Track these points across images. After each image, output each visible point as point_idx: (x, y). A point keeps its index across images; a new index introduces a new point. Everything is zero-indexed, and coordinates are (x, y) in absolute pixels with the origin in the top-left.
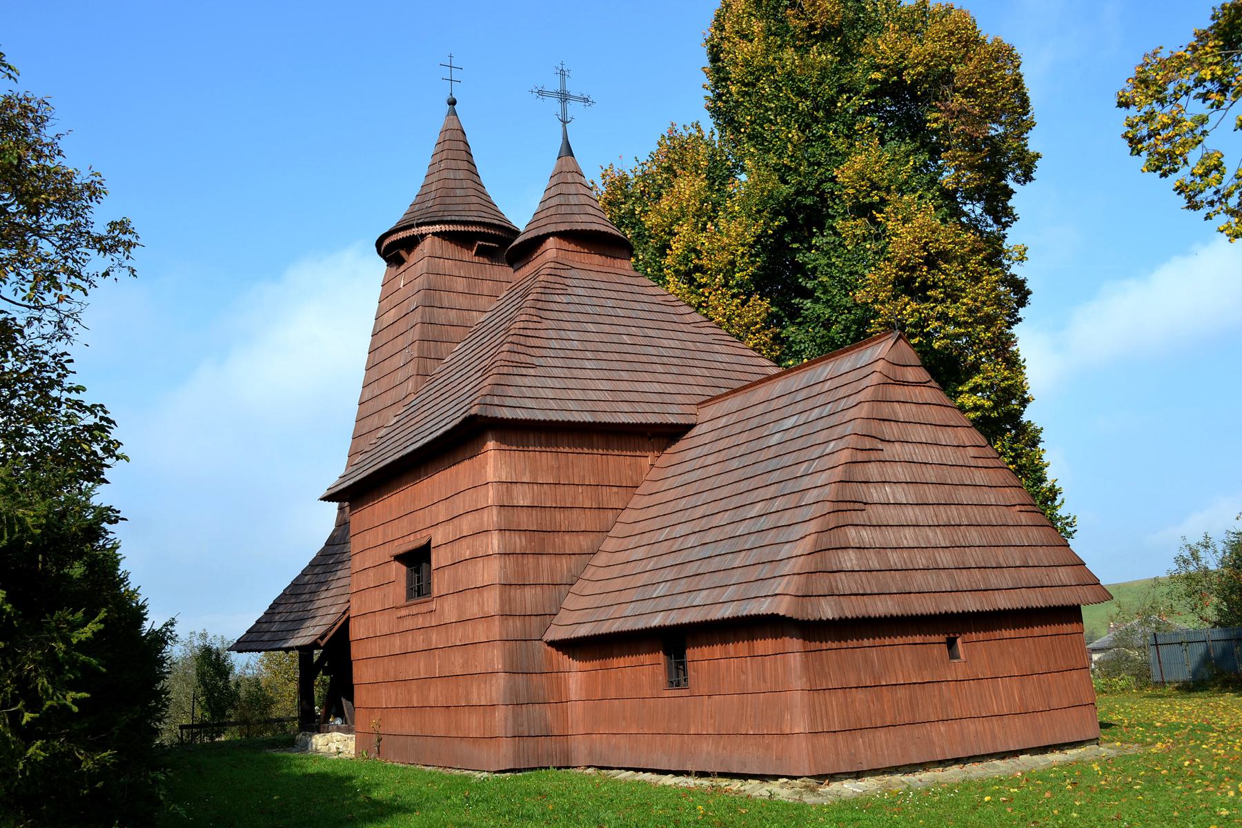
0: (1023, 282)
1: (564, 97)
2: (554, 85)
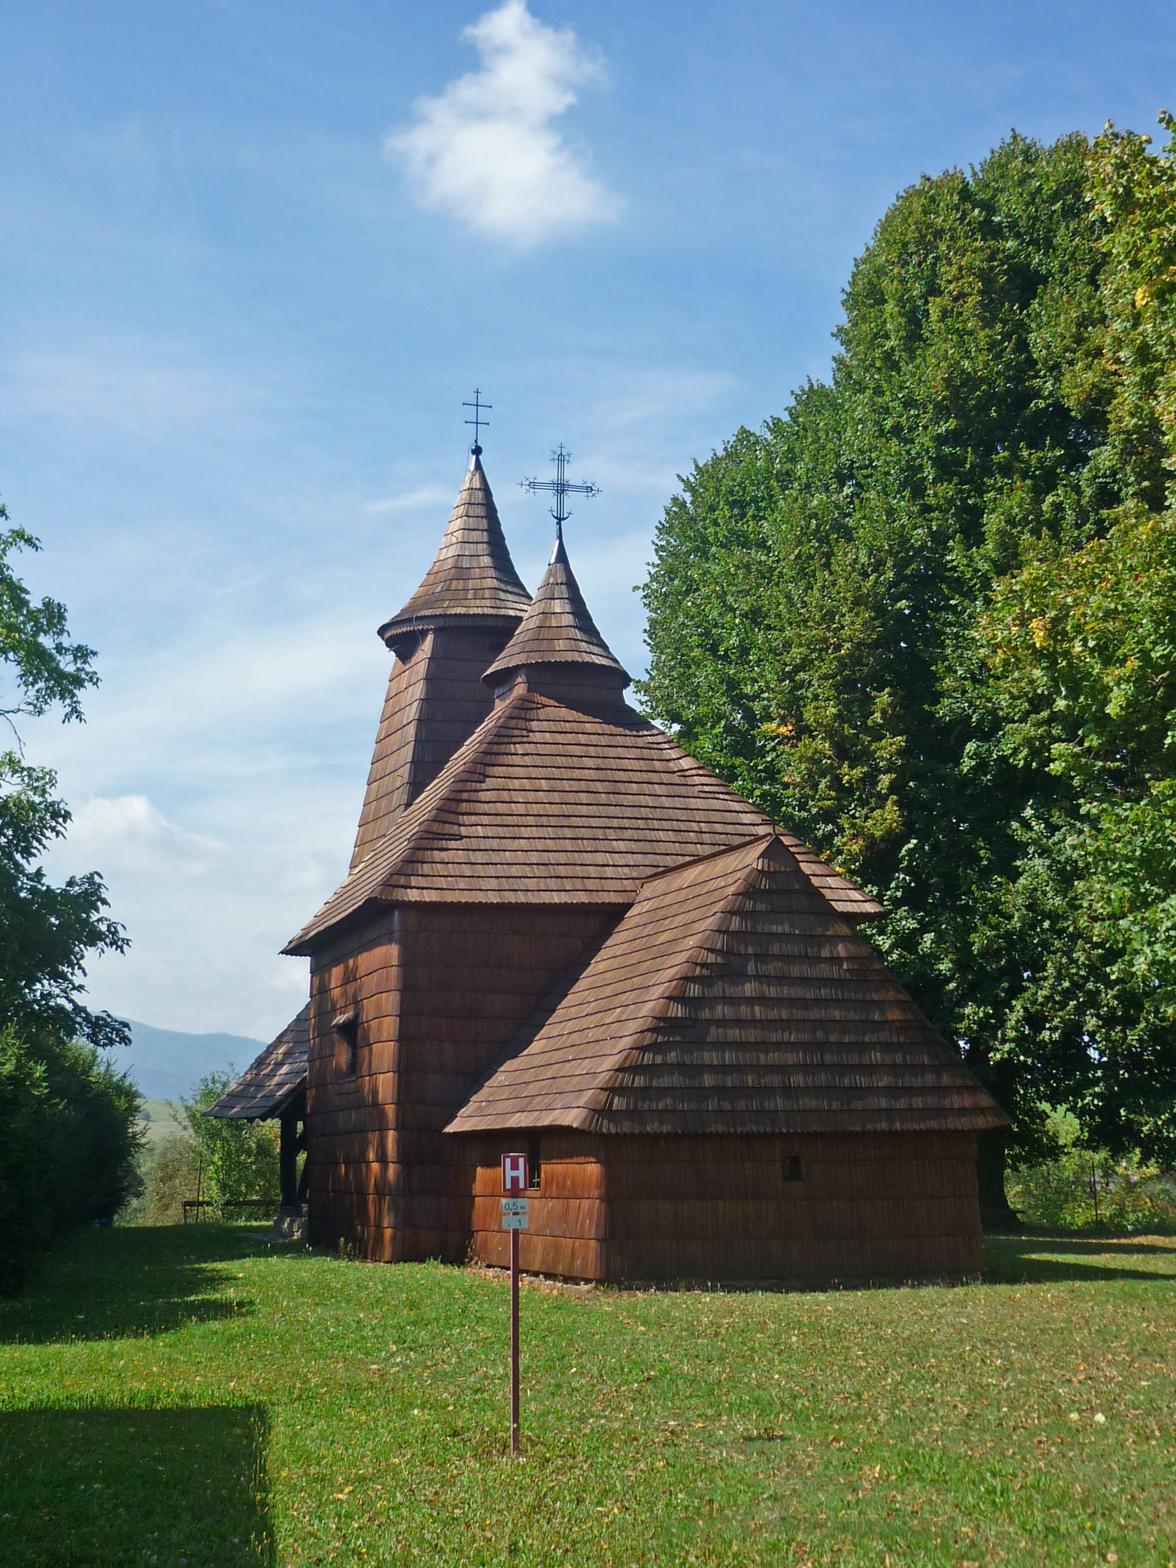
1: (561, 488)
2: (549, 474)
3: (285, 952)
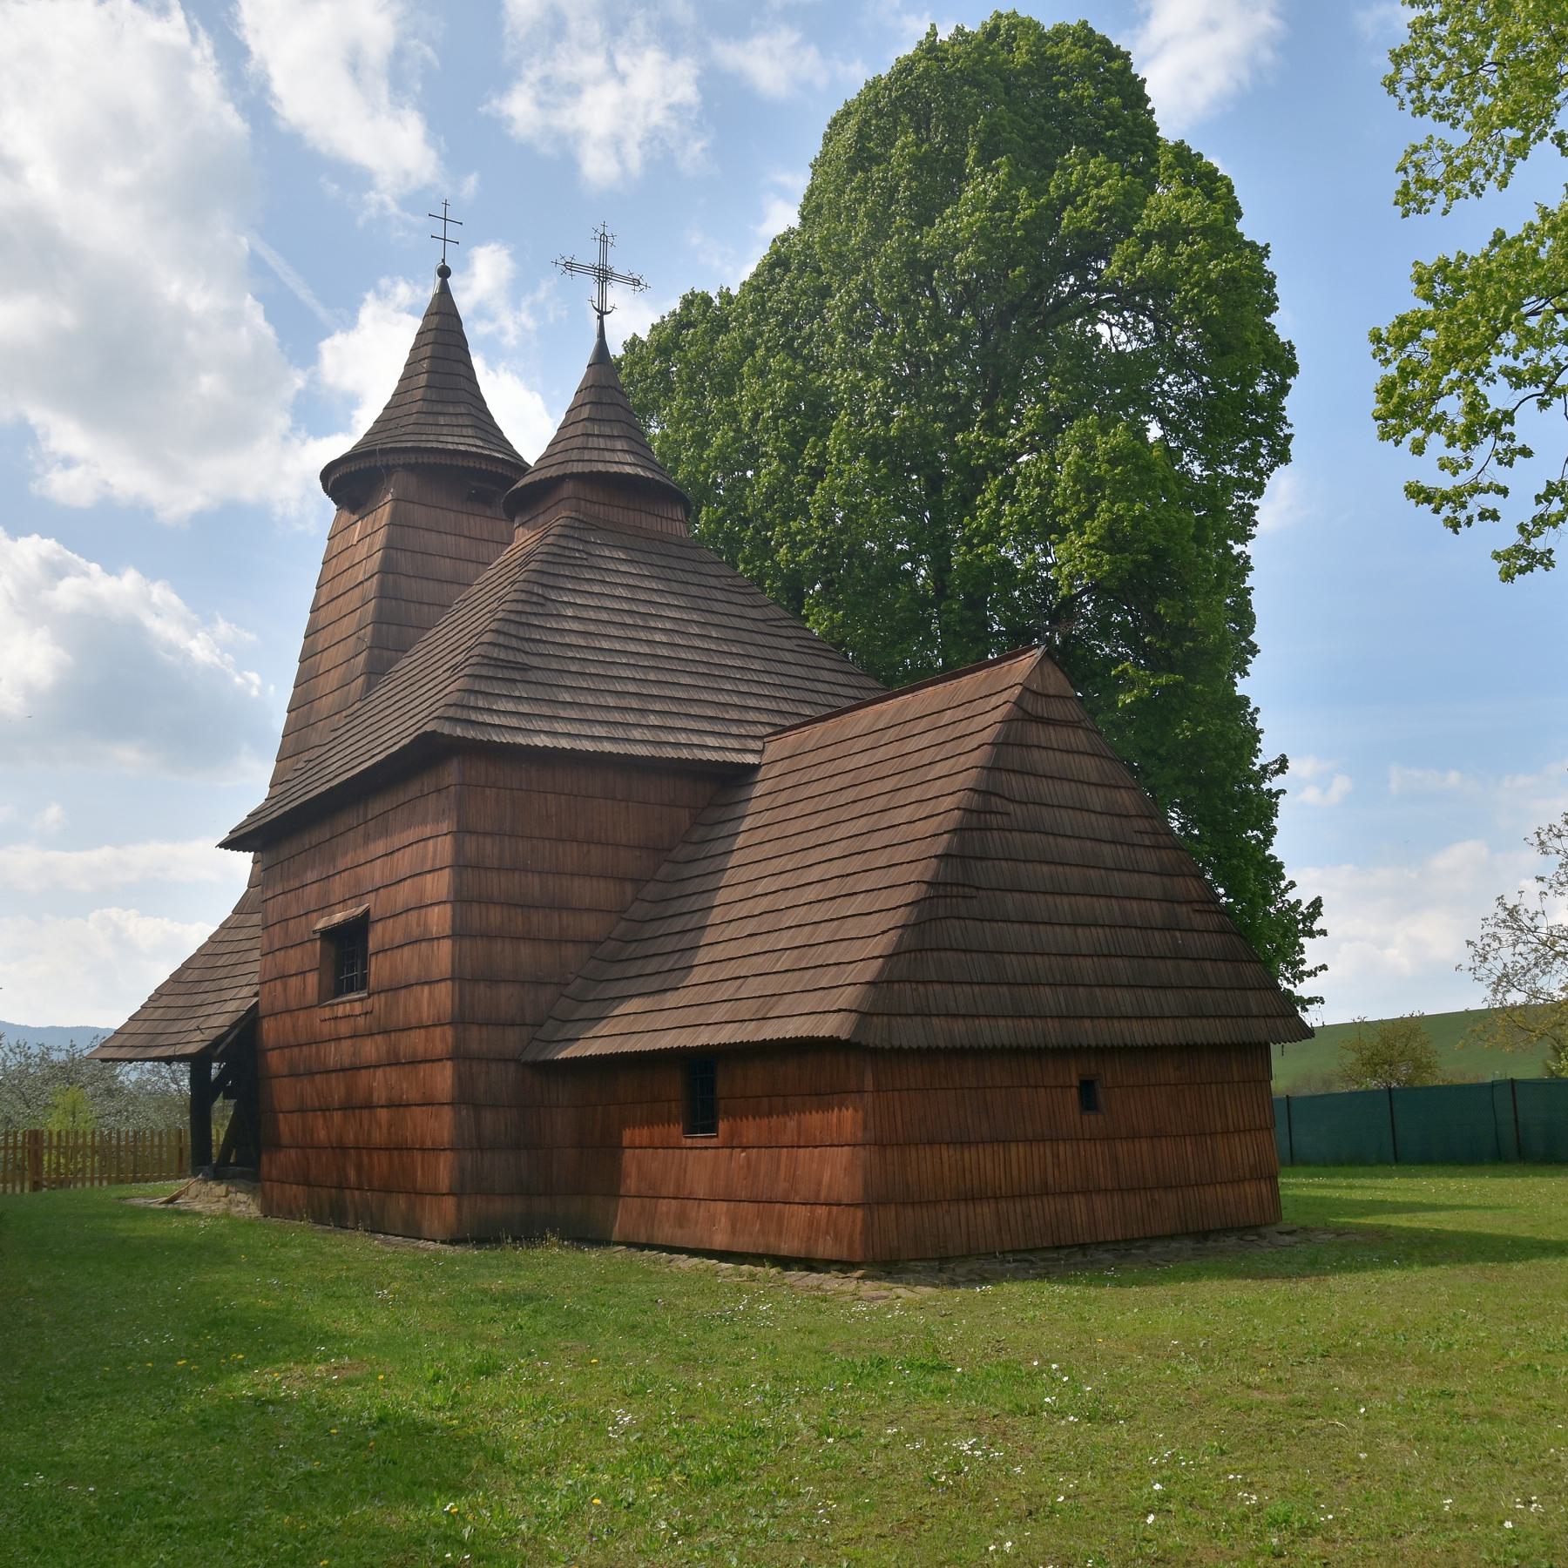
0: (1265, 252)
2: (589, 255)
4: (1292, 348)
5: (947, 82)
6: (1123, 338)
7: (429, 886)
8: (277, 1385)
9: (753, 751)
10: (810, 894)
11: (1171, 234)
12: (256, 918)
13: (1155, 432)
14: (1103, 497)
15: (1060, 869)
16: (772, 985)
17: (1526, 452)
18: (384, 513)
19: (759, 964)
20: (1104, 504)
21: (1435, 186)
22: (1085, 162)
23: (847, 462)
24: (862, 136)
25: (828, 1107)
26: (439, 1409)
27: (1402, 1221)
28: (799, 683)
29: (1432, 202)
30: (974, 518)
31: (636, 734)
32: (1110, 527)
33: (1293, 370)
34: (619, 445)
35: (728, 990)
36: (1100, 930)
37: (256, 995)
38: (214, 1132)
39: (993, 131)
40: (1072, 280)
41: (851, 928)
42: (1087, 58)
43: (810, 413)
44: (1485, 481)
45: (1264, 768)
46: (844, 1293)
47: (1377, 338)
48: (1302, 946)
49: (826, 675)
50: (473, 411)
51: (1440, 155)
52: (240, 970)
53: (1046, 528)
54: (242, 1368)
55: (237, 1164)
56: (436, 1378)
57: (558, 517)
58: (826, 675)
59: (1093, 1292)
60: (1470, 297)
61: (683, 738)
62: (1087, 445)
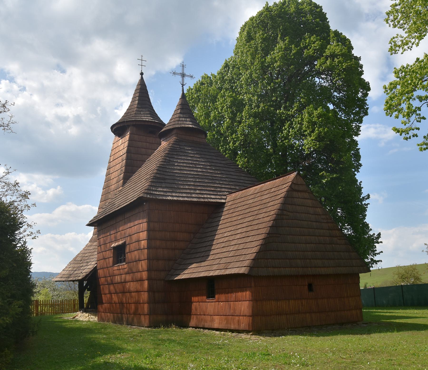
0: (360, 59)
1: (183, 75)
3: (88, 225)
4: (369, 83)
5: (272, 18)
6: (323, 81)
7: (141, 236)
8: (109, 359)
9: (224, 199)
10: (238, 236)
11: (333, 56)
12: (95, 243)
13: (331, 107)
14: (316, 127)
15: (302, 229)
16: (228, 260)
17: (424, 118)
18: (127, 137)
19: (226, 254)
20: (316, 129)
21: (399, 46)
22: (310, 37)
23: (248, 119)
24: (248, 33)
25: (243, 291)
26: (148, 364)
27: (397, 321)
28: (236, 180)
29: (399, 51)
30: (282, 133)
31: (194, 195)
32: (319, 134)
33: (369, 89)
34: (188, 120)
35: (217, 261)
36: (313, 245)
37: (96, 264)
38: (85, 300)
39: (285, 29)
40: (308, 66)
41: (248, 245)
42: (311, 9)
43: (238, 105)
44: (413, 127)
45: (363, 198)
46: (247, 338)
47: (385, 88)
48: (375, 246)
49: (242, 178)
50: (150, 110)
51: (401, 39)
52: (91, 257)
53: (301, 135)
54: (100, 356)
55: (90, 308)
56: (147, 357)
57: (173, 139)
58: (242, 178)
59: (310, 338)
60: (408, 77)
61: (205, 196)
62: (310, 114)
